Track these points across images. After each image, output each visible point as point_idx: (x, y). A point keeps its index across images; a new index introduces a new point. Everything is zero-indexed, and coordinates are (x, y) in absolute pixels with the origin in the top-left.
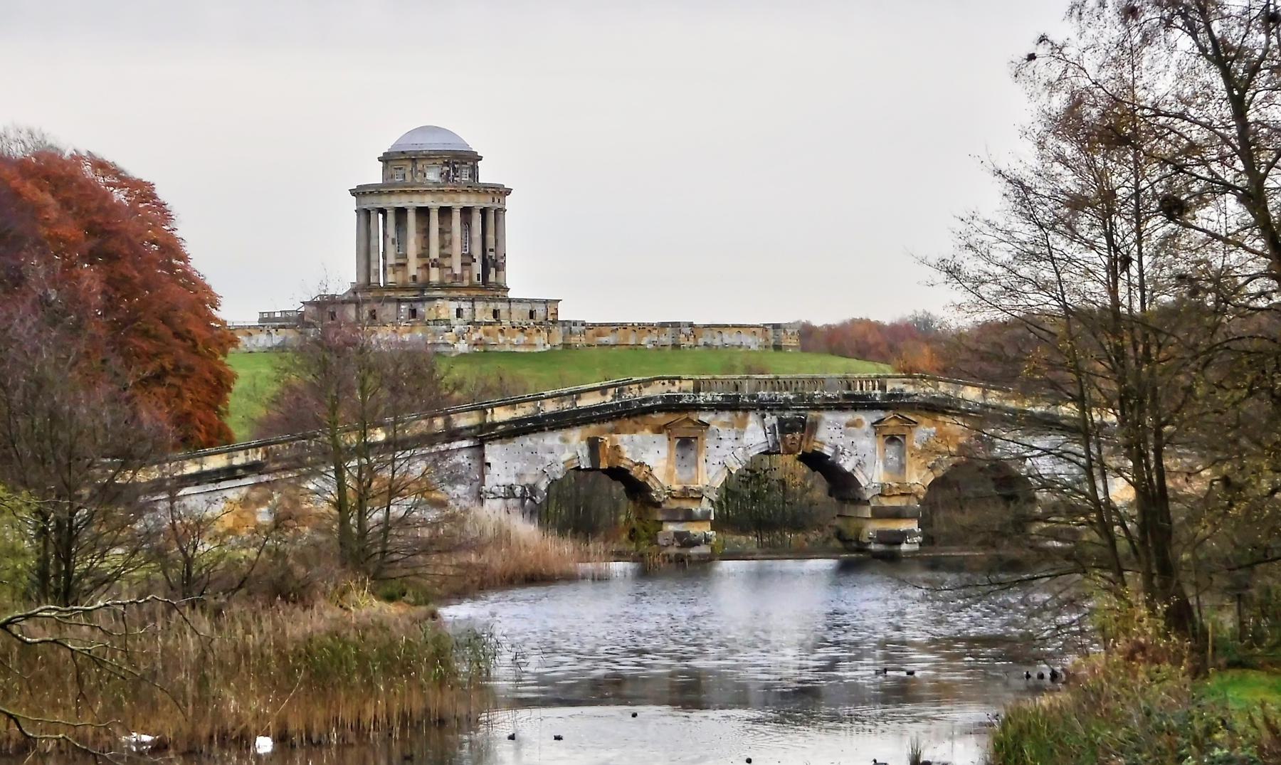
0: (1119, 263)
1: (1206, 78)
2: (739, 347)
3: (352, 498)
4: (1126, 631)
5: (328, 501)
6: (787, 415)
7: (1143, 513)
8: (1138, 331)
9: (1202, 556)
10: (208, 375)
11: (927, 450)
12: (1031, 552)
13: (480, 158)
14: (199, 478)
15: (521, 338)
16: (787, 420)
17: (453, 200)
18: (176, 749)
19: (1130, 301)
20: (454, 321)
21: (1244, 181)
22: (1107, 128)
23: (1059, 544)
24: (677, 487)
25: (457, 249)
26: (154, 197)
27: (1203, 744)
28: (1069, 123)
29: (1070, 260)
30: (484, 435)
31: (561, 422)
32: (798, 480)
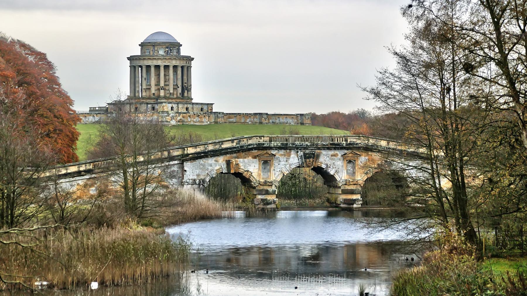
0: (446, 90)
1: (483, 14)
2: (287, 123)
3: (130, 185)
4: (449, 241)
5: (120, 185)
6: (307, 151)
7: (455, 193)
8: (453, 118)
9: (479, 211)
10: (68, 133)
11: (365, 166)
12: (409, 208)
13: (181, 45)
14: (66, 175)
15: (197, 119)
16: (307, 154)
17: (170, 62)
18: (58, 287)
19: (449, 105)
20: (170, 112)
21: (499, 56)
22: (441, 35)
23: (418, 205)
24: (262, 180)
25: (171, 83)
26: (46, 59)
27: (483, 290)
28: (425, 33)
29: (425, 89)
30: (184, 159)
31: (215, 153)
32: (311, 178)
